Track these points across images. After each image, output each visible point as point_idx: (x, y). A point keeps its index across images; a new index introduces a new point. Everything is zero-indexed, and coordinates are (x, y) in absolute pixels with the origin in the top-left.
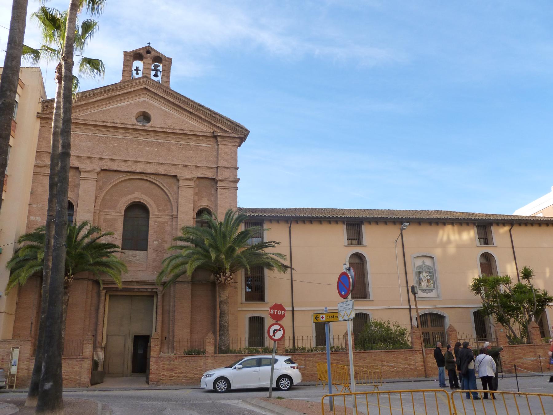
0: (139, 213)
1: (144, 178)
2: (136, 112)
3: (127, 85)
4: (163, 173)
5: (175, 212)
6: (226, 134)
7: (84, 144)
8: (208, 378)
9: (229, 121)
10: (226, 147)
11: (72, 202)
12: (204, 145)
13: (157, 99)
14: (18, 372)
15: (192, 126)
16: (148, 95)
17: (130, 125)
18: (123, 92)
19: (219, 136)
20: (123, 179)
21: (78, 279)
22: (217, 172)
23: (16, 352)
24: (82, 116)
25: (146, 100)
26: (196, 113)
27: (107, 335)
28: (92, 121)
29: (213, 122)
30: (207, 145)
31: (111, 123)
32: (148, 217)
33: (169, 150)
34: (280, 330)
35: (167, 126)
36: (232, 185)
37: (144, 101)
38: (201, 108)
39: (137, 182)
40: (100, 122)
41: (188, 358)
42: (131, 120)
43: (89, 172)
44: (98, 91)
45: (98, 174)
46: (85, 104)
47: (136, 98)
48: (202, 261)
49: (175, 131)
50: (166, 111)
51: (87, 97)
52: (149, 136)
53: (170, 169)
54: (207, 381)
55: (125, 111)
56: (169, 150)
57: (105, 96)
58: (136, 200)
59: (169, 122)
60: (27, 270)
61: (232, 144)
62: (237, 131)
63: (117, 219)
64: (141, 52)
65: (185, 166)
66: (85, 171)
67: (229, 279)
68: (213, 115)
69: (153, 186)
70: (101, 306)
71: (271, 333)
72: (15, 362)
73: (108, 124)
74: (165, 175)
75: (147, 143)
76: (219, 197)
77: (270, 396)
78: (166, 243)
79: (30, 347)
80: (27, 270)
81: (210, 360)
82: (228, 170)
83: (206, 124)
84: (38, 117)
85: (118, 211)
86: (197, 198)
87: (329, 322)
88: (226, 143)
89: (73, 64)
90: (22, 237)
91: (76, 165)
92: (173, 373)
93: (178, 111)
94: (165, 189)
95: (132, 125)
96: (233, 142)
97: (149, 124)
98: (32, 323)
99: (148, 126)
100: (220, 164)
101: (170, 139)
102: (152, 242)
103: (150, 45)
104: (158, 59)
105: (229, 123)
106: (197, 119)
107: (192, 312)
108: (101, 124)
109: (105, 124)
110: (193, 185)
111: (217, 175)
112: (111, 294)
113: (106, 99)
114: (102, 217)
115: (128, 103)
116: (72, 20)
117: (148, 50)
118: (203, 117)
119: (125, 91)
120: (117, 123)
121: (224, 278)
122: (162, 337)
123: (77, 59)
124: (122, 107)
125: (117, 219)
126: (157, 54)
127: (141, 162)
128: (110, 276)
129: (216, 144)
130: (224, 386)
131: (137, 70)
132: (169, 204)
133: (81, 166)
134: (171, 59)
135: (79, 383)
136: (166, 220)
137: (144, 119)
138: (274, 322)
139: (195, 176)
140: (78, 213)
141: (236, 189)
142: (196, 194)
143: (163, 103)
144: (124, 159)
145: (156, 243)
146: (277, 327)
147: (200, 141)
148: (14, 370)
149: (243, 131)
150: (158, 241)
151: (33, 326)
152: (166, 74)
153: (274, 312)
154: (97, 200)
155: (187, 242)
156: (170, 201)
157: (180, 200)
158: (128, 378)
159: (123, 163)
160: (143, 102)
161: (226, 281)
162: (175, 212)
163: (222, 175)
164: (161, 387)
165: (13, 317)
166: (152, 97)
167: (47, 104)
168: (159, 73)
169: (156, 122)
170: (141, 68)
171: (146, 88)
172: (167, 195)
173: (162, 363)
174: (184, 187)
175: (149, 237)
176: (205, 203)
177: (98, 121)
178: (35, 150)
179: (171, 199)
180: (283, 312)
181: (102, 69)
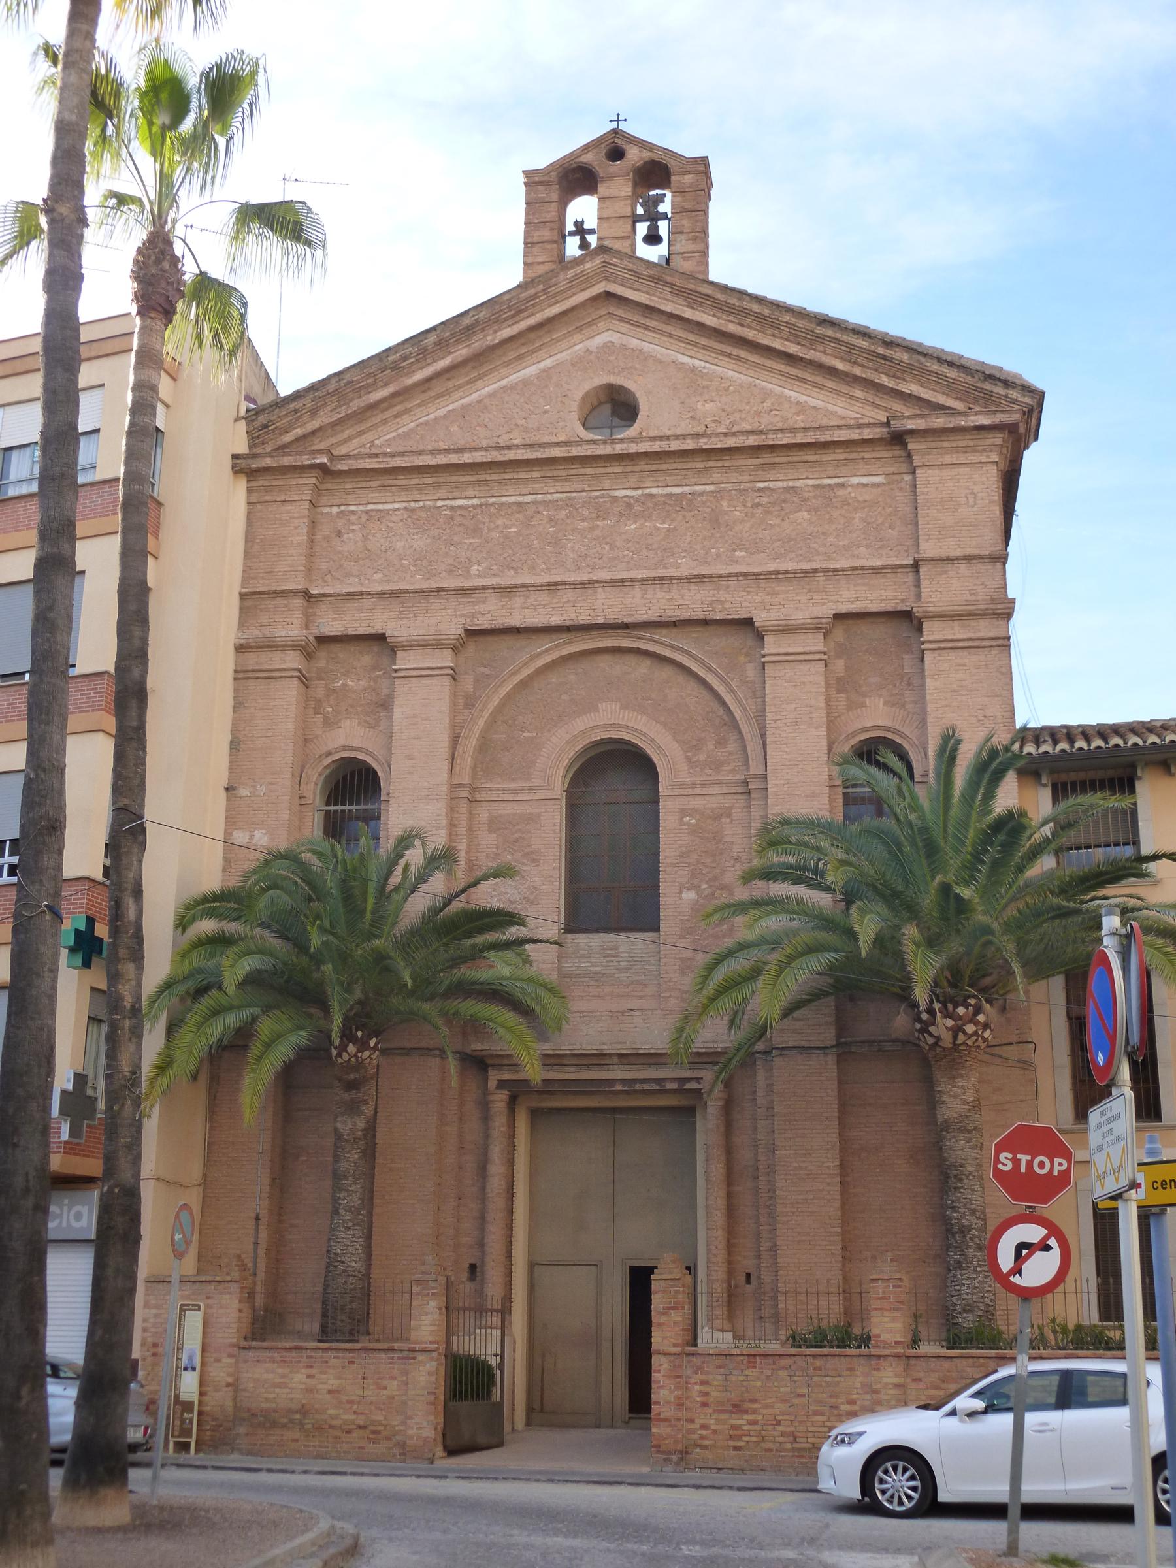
0: (617, 786)
1: (625, 643)
2: (578, 395)
3: (535, 296)
4: (699, 615)
5: (756, 769)
6: (939, 422)
7: (399, 545)
8: (843, 1451)
9: (951, 364)
10: (947, 473)
11: (375, 765)
12: (855, 480)
13: (654, 330)
14: (201, 1394)
15: (802, 408)
16: (622, 320)
17: (558, 444)
18: (523, 325)
19: (912, 432)
20: (548, 659)
21: (407, 1052)
22: (918, 585)
23: (194, 1321)
24: (388, 443)
26: (810, 355)
27: (532, 1266)
28: (421, 453)
29: (885, 380)
30: (866, 478)
31: (486, 449)
32: (655, 800)
33: (715, 521)
34: (1048, 1248)
35: (700, 429)
36: (985, 629)
37: (608, 347)
38: (830, 332)
39: (604, 662)
40: (448, 451)
41: (801, 1362)
42: (565, 427)
43: (424, 645)
45: (456, 650)
46: (395, 395)
47: (577, 337)
48: (831, 956)
49: (731, 442)
50: (693, 369)
51: (395, 367)
52: (633, 478)
53: (722, 595)
54: (840, 1466)
55: (539, 398)
56: (715, 521)
57: (462, 352)
58: (606, 735)
59: (707, 408)
60: (200, 1025)
61: (974, 458)
62: (988, 399)
63: (539, 816)
64: (587, 158)
65: (777, 576)
66: (409, 646)
67: (970, 1028)
68: (881, 350)
69: (667, 672)
70: (496, 1151)
71: (1006, 1261)
72: (191, 1358)
73: (479, 457)
74: (705, 623)
75: (629, 506)
76: (930, 684)
77: (1012, 1549)
79: (235, 1304)
80: (200, 1025)
81: (889, 1374)
82: (963, 568)
83: (858, 393)
84: (237, 471)
85: (536, 783)
86: (841, 701)
87: (1163, 1208)
88: (948, 459)
89: (83, 221)
90: (188, 907)
91: (377, 628)
92: (742, 1421)
93: (738, 358)
94: (710, 678)
95: (567, 443)
96: (974, 449)
97: (632, 432)
98: (257, 1218)
99: (628, 439)
100: (928, 549)
102: (677, 897)
103: (623, 126)
104: (656, 171)
105: (952, 373)
106: (819, 379)
107: (844, 1167)
108: (454, 459)
109: (467, 458)
110: (820, 647)
111: (918, 596)
112: (534, 1104)
113: (464, 362)
114: (483, 813)
115: (548, 363)
116: (76, 57)
117: (614, 146)
118: (840, 365)
119: (532, 321)
120: (509, 448)
121: (950, 1023)
122: (730, 1273)
123: (92, 195)
124: (526, 383)
125: (539, 816)
126: (647, 155)
127: (612, 582)
128: (507, 1034)
129: (904, 467)
130: (903, 1487)
131: (580, 230)
132: (733, 736)
133: (395, 629)
134: (704, 161)
135: (402, 1445)
136: (726, 802)
137: (614, 413)
138: (1021, 1207)
139: (826, 611)
140: (393, 806)
141: (1003, 643)
142: (839, 685)
143: (679, 339)
144: (545, 578)
145: (691, 895)
146: (1032, 1233)
147: (838, 464)
148: (189, 1384)
149: (1014, 394)
150: (696, 888)
151: (263, 1228)
152: (686, 223)
153: (1016, 1162)
154: (460, 749)
155: (797, 881)
156: (735, 725)
157: (770, 717)
158: (612, 1432)
159: (543, 597)
160: (606, 348)
161: (961, 1038)
162: (756, 769)
163: (941, 591)
164: (695, 1476)
165: (193, 1198)
166: (637, 325)
167: (262, 419)
168: (663, 227)
169: (660, 418)
170: (591, 223)
171: (608, 295)
172: (723, 703)
173: (699, 1377)
174: (786, 659)
176: (875, 715)
177: (440, 452)
178: (237, 589)
179: (738, 714)
180: (1059, 1165)
181: (312, 235)
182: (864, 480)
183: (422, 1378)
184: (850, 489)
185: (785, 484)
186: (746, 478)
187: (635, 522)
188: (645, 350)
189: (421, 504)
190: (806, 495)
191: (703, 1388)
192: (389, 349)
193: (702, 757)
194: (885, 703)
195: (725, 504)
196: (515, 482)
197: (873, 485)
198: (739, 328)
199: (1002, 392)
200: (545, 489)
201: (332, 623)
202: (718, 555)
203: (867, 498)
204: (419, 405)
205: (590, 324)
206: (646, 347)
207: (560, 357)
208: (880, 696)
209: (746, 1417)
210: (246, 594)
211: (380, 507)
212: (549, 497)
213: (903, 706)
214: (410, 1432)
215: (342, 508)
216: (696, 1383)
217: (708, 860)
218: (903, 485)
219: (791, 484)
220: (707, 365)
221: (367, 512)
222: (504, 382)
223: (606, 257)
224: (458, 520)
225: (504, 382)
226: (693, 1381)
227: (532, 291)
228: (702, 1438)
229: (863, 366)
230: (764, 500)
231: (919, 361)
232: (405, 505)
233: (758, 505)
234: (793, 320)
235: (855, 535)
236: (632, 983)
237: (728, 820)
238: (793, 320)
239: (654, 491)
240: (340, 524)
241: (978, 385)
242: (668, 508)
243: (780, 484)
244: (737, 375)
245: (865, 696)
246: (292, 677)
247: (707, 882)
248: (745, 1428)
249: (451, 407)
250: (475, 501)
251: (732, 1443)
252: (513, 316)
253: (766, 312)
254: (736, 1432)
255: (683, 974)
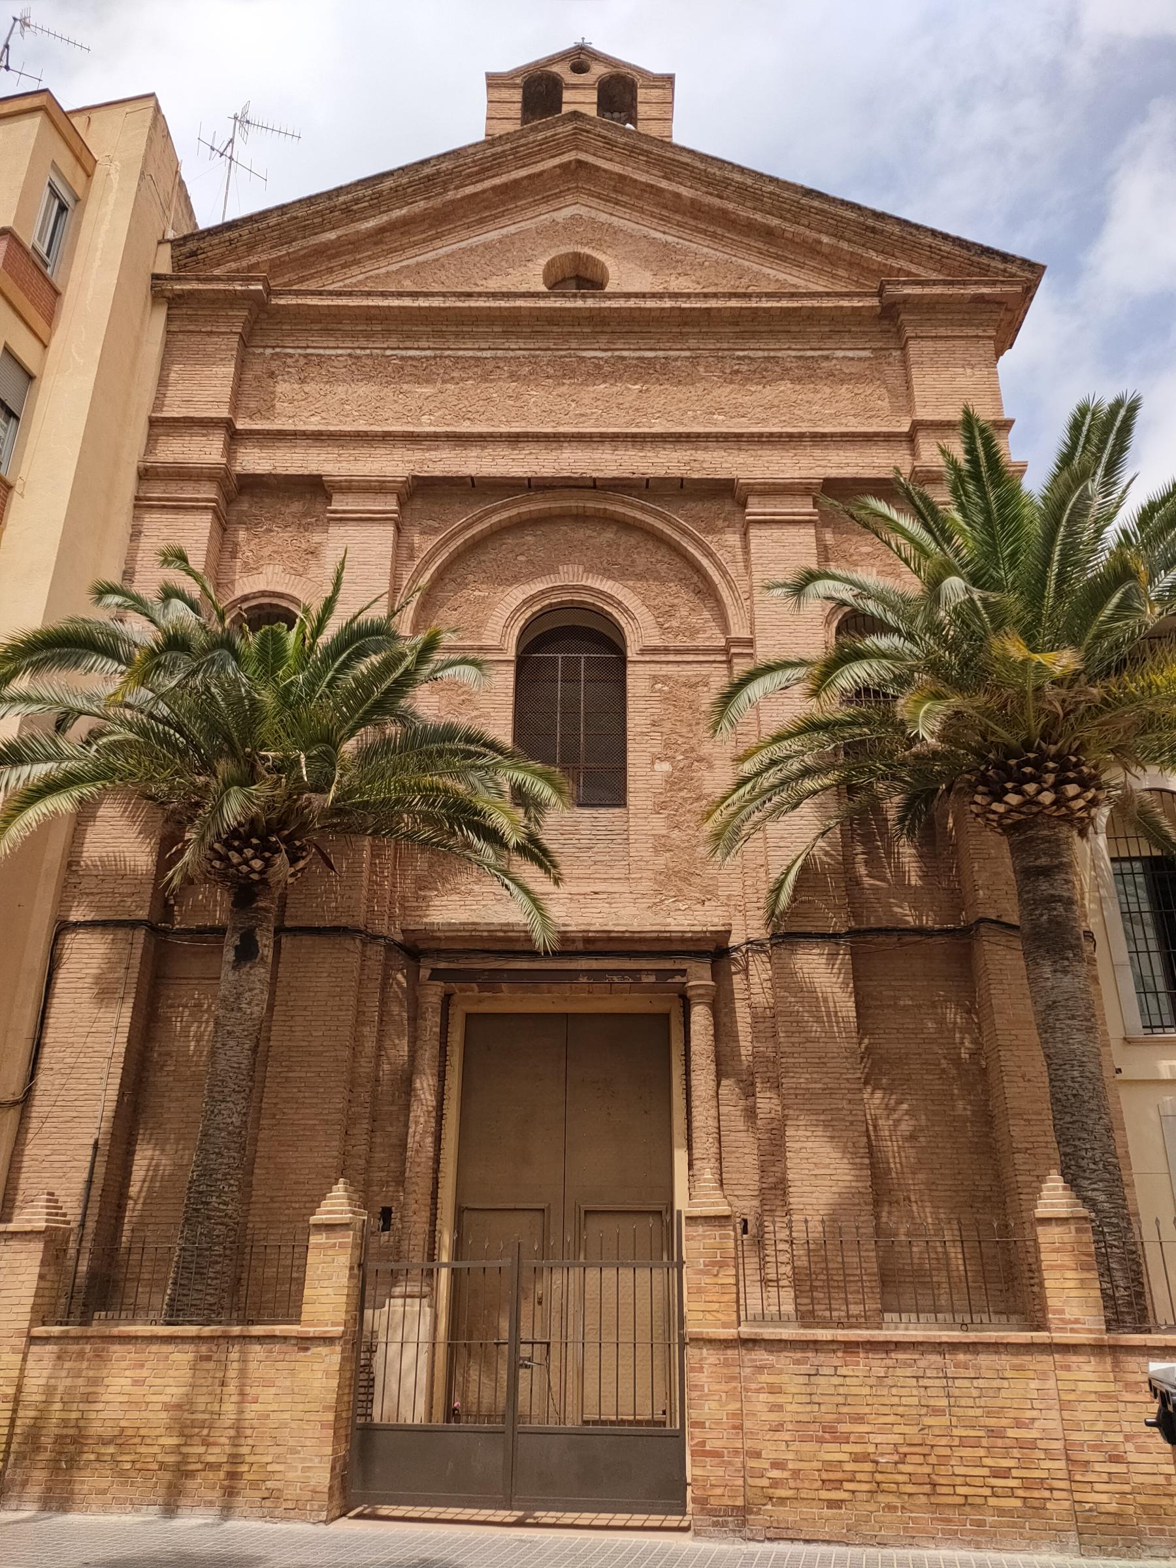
12: (840, 354)
25: (583, 211)
38: (816, 204)
44: (388, 184)
47: (543, 208)
50: (666, 244)
52: (603, 339)
53: (700, 455)
61: (971, 332)
64: (555, 69)
68: (870, 222)
75: (599, 367)
78: (710, 767)
88: (942, 332)
101: (692, 343)
115: (512, 229)
124: (487, 246)
134: (670, 79)
145: (666, 767)
149: (1013, 269)
150: (668, 758)
175: (630, 746)
182: (850, 354)
183: (316, 1384)
184: (834, 362)
185: (766, 354)
186: (725, 346)
187: (605, 382)
188: (615, 224)
189: (368, 351)
190: (788, 365)
191: (772, 1398)
192: (341, 188)
193: (675, 624)
194: (878, 573)
195: (702, 370)
196: (473, 336)
197: (860, 359)
198: (718, 200)
199: (1001, 266)
200: (506, 345)
201: (255, 461)
202: (695, 418)
203: (853, 371)
204: (370, 258)
205: (557, 196)
206: (616, 221)
207: (524, 225)
208: (873, 565)
209: (846, 1448)
210: (158, 420)
211: (321, 352)
212: (511, 354)
213: (899, 576)
214: (291, 1475)
215: (278, 350)
216: (758, 1391)
217: (684, 730)
218: (891, 360)
219: (772, 354)
220: (681, 241)
221: (306, 356)
222: (463, 244)
223: (579, 124)
224: (408, 369)
225: (463, 244)
226: (753, 1386)
227: (499, 149)
228: (775, 1483)
229: (849, 241)
230: (744, 368)
231: (911, 234)
232: (349, 351)
233: (737, 372)
234: (778, 191)
235: (842, 405)
236: (595, 863)
237: (706, 689)
238: (778, 191)
239: (625, 354)
240: (274, 365)
241: (975, 258)
242: (639, 370)
243: (760, 354)
244: (713, 252)
245: (856, 565)
246: (206, 508)
247: (683, 753)
248: (849, 1467)
249: (405, 263)
250: (428, 353)
251: (825, 1495)
252: (477, 173)
253: (749, 182)
254: (832, 1476)
255: (656, 851)
